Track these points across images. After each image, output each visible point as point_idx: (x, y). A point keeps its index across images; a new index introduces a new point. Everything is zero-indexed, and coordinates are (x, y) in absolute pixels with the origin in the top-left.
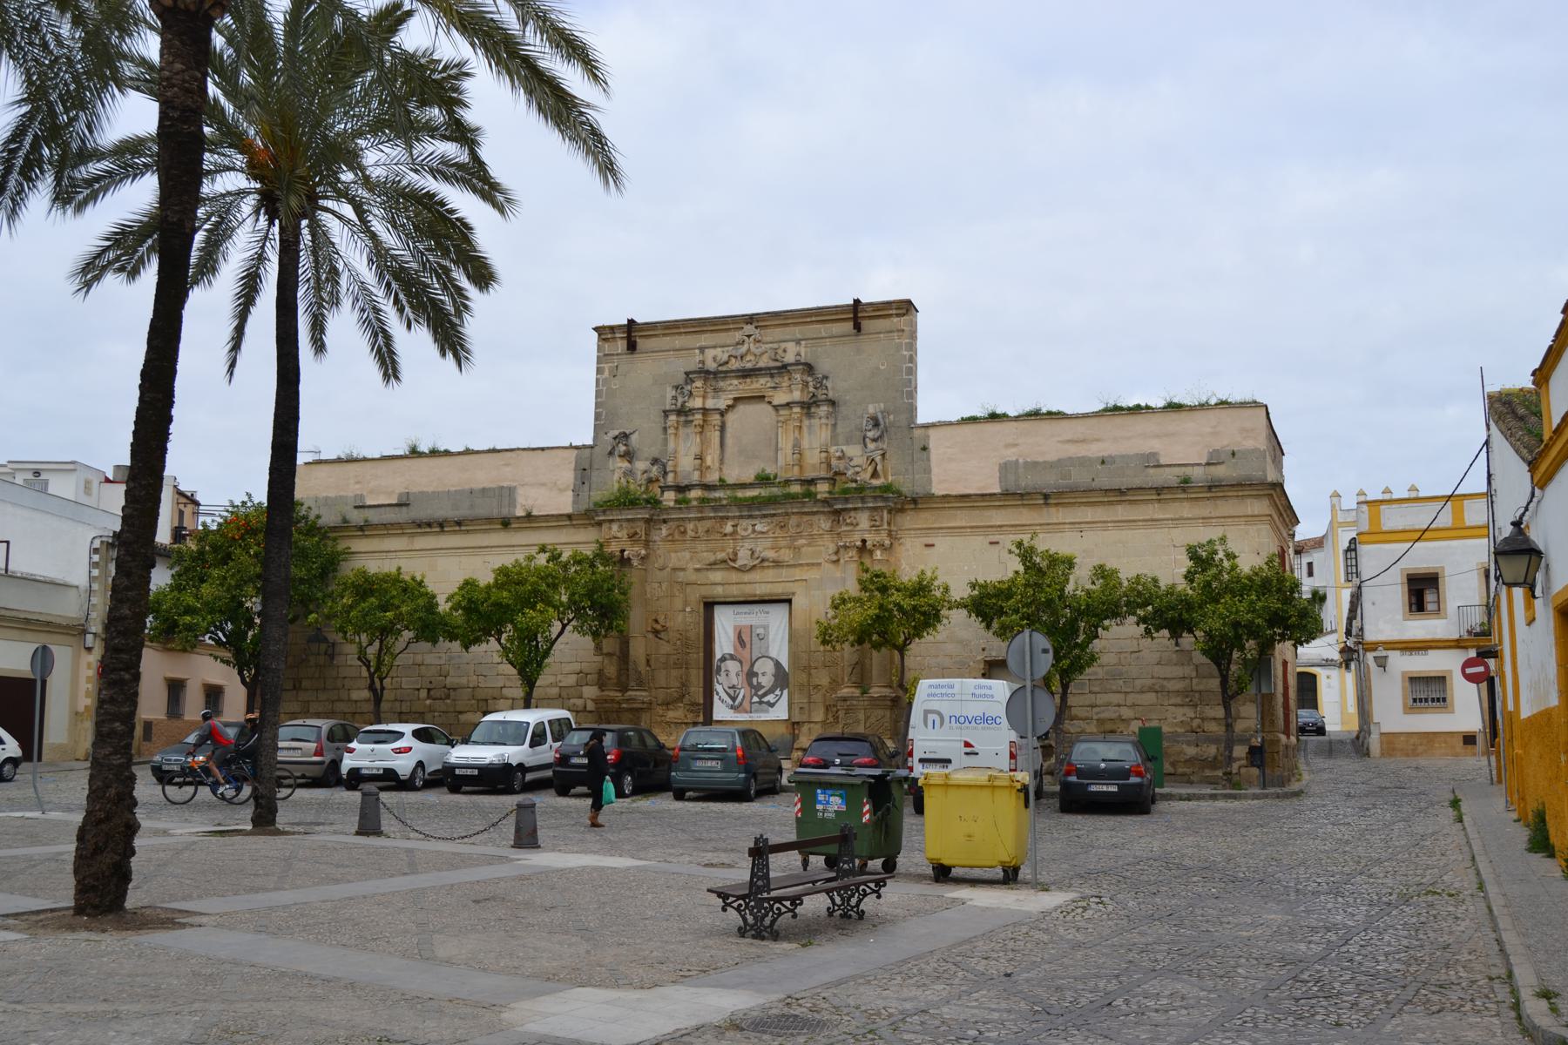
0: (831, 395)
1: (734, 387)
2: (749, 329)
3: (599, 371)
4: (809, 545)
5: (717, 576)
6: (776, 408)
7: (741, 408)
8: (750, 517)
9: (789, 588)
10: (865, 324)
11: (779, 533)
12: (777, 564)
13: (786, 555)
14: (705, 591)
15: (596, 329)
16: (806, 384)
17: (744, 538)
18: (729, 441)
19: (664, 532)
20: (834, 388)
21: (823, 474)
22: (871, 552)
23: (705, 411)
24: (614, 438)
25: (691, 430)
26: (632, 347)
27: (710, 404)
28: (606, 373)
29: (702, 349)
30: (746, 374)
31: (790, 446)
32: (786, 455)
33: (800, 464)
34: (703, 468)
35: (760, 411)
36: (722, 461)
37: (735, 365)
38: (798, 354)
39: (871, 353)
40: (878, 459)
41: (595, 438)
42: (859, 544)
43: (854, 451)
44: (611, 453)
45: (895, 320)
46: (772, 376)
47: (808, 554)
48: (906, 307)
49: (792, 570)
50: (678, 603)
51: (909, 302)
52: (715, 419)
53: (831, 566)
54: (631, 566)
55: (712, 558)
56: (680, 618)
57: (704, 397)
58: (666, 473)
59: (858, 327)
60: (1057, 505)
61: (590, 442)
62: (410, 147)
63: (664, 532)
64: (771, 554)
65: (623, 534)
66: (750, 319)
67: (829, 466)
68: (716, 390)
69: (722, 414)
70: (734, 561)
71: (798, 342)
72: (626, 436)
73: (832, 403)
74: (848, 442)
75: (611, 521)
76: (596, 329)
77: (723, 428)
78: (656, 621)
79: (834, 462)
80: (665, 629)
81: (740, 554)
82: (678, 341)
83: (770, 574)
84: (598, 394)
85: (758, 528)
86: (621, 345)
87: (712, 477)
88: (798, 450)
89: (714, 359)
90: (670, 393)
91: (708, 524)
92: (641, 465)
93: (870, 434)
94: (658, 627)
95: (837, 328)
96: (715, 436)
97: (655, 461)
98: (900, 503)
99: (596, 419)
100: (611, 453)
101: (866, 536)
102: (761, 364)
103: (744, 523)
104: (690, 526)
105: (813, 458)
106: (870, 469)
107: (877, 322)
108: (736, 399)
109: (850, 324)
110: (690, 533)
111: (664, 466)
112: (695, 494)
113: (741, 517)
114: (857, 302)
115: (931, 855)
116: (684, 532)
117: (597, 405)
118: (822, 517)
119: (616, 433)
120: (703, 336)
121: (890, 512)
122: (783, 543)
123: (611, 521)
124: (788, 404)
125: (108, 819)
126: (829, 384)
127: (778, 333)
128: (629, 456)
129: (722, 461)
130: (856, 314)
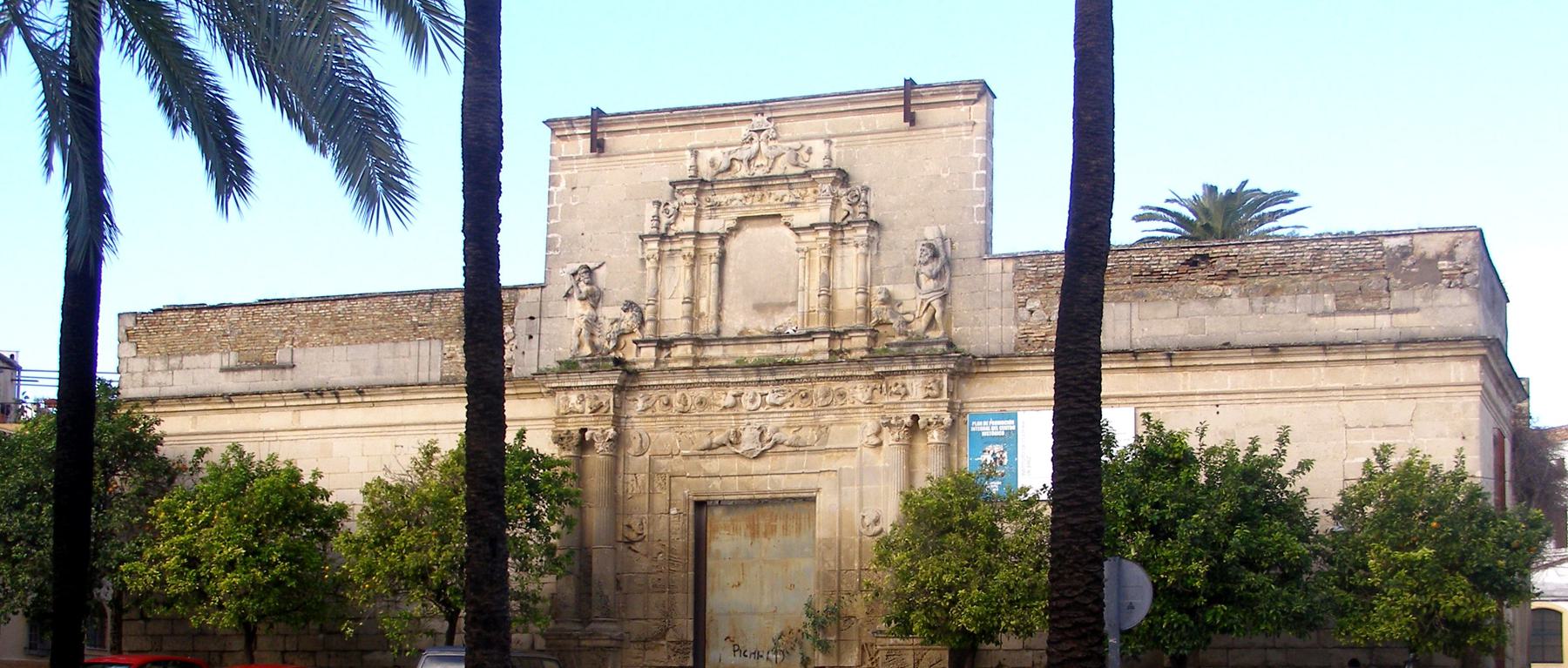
2: (760, 121)
4: (840, 423)
5: (713, 465)
6: (796, 230)
10: (920, 114)
12: (797, 448)
13: (808, 435)
26: (598, 147)
30: (755, 184)
40: (936, 304)
42: (908, 420)
63: (640, 404)
64: (788, 436)
67: (868, 312)
68: (715, 207)
77: (722, 259)
81: (745, 435)
86: (584, 144)
90: (651, 210)
91: (702, 392)
94: (633, 536)
97: (629, 306)
101: (918, 411)
106: (926, 318)
110: (677, 405)
118: (859, 384)
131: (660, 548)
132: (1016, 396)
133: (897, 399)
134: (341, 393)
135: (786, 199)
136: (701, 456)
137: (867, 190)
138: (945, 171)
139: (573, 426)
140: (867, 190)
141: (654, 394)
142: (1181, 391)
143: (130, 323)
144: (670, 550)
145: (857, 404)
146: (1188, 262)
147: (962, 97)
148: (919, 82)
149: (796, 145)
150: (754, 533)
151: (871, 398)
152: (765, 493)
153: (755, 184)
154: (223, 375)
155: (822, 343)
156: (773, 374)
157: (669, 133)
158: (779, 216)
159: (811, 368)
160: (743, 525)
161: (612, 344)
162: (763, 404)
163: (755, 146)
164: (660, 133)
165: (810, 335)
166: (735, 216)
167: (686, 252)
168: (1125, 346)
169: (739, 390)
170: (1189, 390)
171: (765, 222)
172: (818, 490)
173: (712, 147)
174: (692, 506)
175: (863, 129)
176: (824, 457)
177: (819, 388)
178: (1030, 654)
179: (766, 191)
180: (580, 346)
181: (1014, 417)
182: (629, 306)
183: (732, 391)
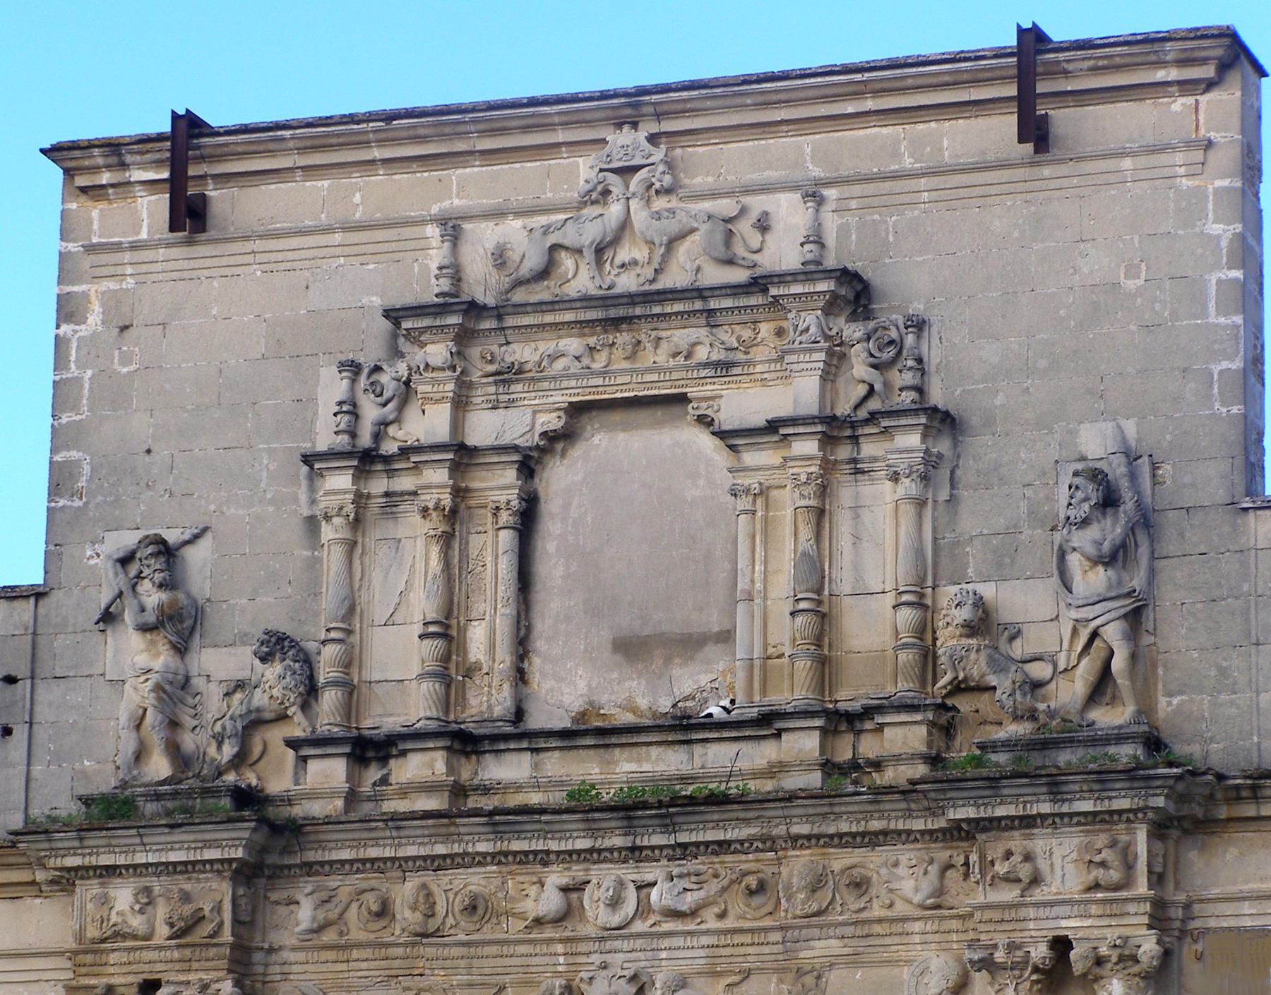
0: (937, 396)
2: (625, 142)
3: (68, 310)
4: (854, 960)
6: (730, 438)
7: (600, 441)
8: (635, 853)
10: (1063, 119)
11: (740, 912)
15: (54, 152)
16: (836, 359)
18: (551, 564)
19: (305, 914)
20: (961, 364)
21: (904, 687)
26: (189, 216)
27: (484, 427)
28: (94, 319)
30: (616, 314)
33: (825, 666)
34: (451, 671)
36: (522, 645)
37: (579, 278)
38: (816, 239)
40: (1113, 633)
41: (52, 558)
42: (1040, 952)
43: (1026, 601)
44: (108, 617)
45: (1180, 104)
51: (1231, 37)
57: (461, 404)
58: (311, 691)
59: (1036, 132)
61: (33, 575)
62: (1036, 969)
63: (305, 914)
67: (928, 657)
68: (508, 375)
69: (528, 464)
72: (166, 552)
73: (944, 422)
74: (1001, 570)
76: (54, 152)
77: (527, 519)
79: (948, 641)
82: (364, 194)
84: (62, 395)
86: (151, 210)
87: (487, 701)
88: (821, 613)
89: (500, 258)
91: (475, 880)
92: (219, 663)
93: (1084, 539)
96: (493, 550)
97: (276, 645)
99: (55, 489)
100: (108, 617)
101: (1068, 925)
102: (676, 278)
103: (604, 877)
104: (404, 892)
105: (873, 628)
108: (577, 410)
109: (1008, 123)
110: (407, 916)
111: (307, 661)
112: (423, 765)
113: (594, 855)
115: (416, 670)
117: (58, 439)
118: (907, 855)
119: (129, 539)
120: (456, 175)
122: (753, 954)
124: (773, 426)
126: (934, 354)
129: (522, 645)
133: (1009, 894)
135: (702, 354)
137: (919, 325)
138: (1132, 272)
140: (919, 325)
145: (901, 909)
147: (1173, 74)
149: (726, 206)
151: (940, 891)
157: (380, 178)
158: (682, 399)
161: (229, 750)
162: (643, 909)
163: (615, 210)
164: (356, 179)
166: (562, 399)
167: (429, 499)
169: (578, 872)
171: (642, 415)
173: (498, 214)
175: (908, 162)
177: (798, 865)
179: (644, 333)
180: (140, 755)
182: (276, 645)
183: (556, 877)
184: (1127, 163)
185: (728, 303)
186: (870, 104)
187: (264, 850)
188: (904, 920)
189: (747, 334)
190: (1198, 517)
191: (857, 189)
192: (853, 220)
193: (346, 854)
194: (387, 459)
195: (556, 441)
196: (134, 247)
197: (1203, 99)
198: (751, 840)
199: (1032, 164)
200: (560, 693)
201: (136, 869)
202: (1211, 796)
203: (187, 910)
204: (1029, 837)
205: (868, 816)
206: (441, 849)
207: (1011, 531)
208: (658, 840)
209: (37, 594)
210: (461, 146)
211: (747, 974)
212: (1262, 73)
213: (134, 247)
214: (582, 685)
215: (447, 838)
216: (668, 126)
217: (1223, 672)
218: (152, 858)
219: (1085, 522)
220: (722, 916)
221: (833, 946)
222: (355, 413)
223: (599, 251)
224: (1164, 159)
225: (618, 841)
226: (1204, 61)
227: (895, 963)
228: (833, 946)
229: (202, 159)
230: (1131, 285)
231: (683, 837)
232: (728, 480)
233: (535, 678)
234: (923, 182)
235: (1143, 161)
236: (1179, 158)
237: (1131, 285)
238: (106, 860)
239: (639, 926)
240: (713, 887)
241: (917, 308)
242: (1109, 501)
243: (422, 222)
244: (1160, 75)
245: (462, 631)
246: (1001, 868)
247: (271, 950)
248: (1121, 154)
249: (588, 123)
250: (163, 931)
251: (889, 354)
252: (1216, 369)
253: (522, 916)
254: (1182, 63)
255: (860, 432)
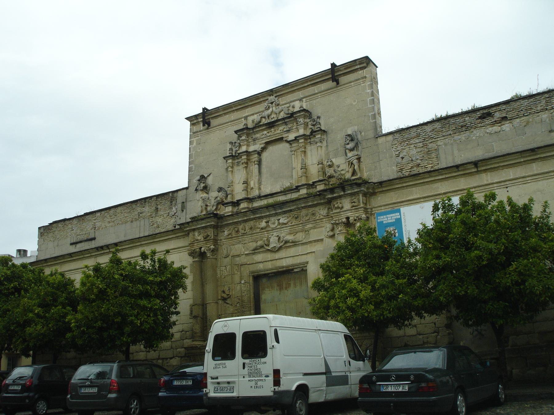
1: (264, 135)
2: (272, 98)
4: (314, 228)
5: (259, 257)
7: (271, 148)
8: (276, 214)
9: (302, 259)
11: (294, 222)
12: (295, 244)
13: (300, 237)
14: (253, 268)
15: (187, 119)
16: (306, 125)
17: (273, 229)
22: (353, 225)
23: (247, 153)
24: (200, 181)
25: (241, 167)
27: (251, 149)
28: (195, 144)
29: (246, 118)
30: (271, 125)
31: (299, 166)
32: (297, 172)
35: (283, 147)
36: (260, 183)
37: (264, 121)
39: (348, 95)
40: (355, 162)
42: (344, 220)
45: (360, 72)
46: (286, 123)
47: (314, 235)
48: (366, 62)
49: (304, 247)
50: (237, 278)
51: (367, 58)
52: (255, 157)
53: (330, 240)
54: (207, 258)
55: (254, 245)
56: (238, 287)
58: (227, 196)
60: (485, 171)
61: (186, 185)
63: (226, 233)
64: (290, 238)
65: (200, 238)
66: (271, 92)
67: (324, 173)
68: (254, 140)
70: (268, 245)
71: (301, 100)
75: (194, 230)
76: (187, 119)
77: (260, 163)
78: (224, 292)
80: (229, 297)
81: (271, 240)
82: (233, 116)
83: (292, 251)
84: (190, 156)
85: (281, 221)
87: (256, 193)
88: (304, 167)
89: (253, 121)
90: (229, 146)
91: (251, 223)
92: (214, 194)
94: (225, 296)
95: (323, 86)
97: (220, 190)
98: (368, 189)
101: (349, 214)
104: (241, 227)
106: (351, 170)
107: (352, 75)
110: (242, 231)
112: (243, 205)
114: (333, 65)
116: (238, 231)
118: (321, 207)
121: (365, 195)
123: (194, 230)
125: (49, 285)
127: (289, 98)
128: (206, 189)
129: (260, 183)
130: (334, 74)
131: (238, 301)
132: (399, 200)
133: (338, 211)
134: (110, 247)
135: (285, 130)
136: (253, 254)
137: (319, 117)
138: (355, 101)
139: (196, 247)
140: (319, 117)
141: (231, 227)
142: (486, 183)
143: (42, 230)
144: (242, 301)
145: (322, 217)
146: (480, 118)
147: (358, 67)
148: (338, 64)
149: (288, 105)
150: (281, 288)
151: (328, 213)
152: (283, 267)
153: (271, 125)
154: (71, 246)
155: (303, 191)
156: (281, 209)
158: (282, 138)
159: (298, 202)
160: (275, 285)
161: (214, 208)
162: (279, 224)
163: (271, 109)
164: (232, 114)
165: (297, 188)
166: (264, 142)
167: (243, 161)
168: (452, 165)
169: (268, 219)
170: (490, 182)
172: (307, 263)
173: (253, 114)
174: (251, 278)
175: (316, 92)
176: (308, 246)
177: (304, 212)
178: (421, 337)
180: (202, 212)
181: (399, 211)
182: (220, 190)
183: (264, 221)
184: (352, 83)
185: (288, 120)
186: (309, 83)
187: (218, 223)
188: (322, 219)
189: (292, 125)
190: (369, 141)
191: (308, 98)
192: (308, 103)
193: (231, 222)
194: (237, 156)
195: (264, 149)
196: (200, 131)
197: (365, 70)
198: (295, 209)
199: (337, 87)
200: (267, 189)
201: (198, 229)
202: (373, 188)
203: (206, 234)
204: (341, 200)
205: (313, 201)
206: (245, 218)
207: (337, 149)
208: (280, 211)
209: (187, 188)
210: (247, 105)
211: (297, 233)
212: (377, 67)
213: (200, 131)
214: (270, 188)
215: (246, 216)
216: (278, 94)
217: (376, 167)
218: (199, 226)
219: (348, 144)
220: (291, 223)
221: (311, 226)
222: (232, 150)
223: (268, 117)
224: (358, 81)
225: (274, 212)
226: (363, 63)
227: (321, 227)
228: (311, 226)
229: (208, 115)
230: (354, 103)
231: (284, 210)
232: (290, 149)
233: (262, 189)
234: (319, 94)
235: (355, 83)
236: (361, 81)
237: (354, 103)
238: (193, 228)
239: (278, 227)
240: (290, 218)
241: (319, 115)
242: (352, 140)
243: (242, 118)
244: (356, 67)
245: (250, 182)
246: (336, 206)
247: (221, 240)
248: (351, 82)
249: (265, 97)
250: (202, 238)
251: (315, 123)
252: (370, 114)
253: (259, 228)
254: (360, 64)
255: (376, 191)
